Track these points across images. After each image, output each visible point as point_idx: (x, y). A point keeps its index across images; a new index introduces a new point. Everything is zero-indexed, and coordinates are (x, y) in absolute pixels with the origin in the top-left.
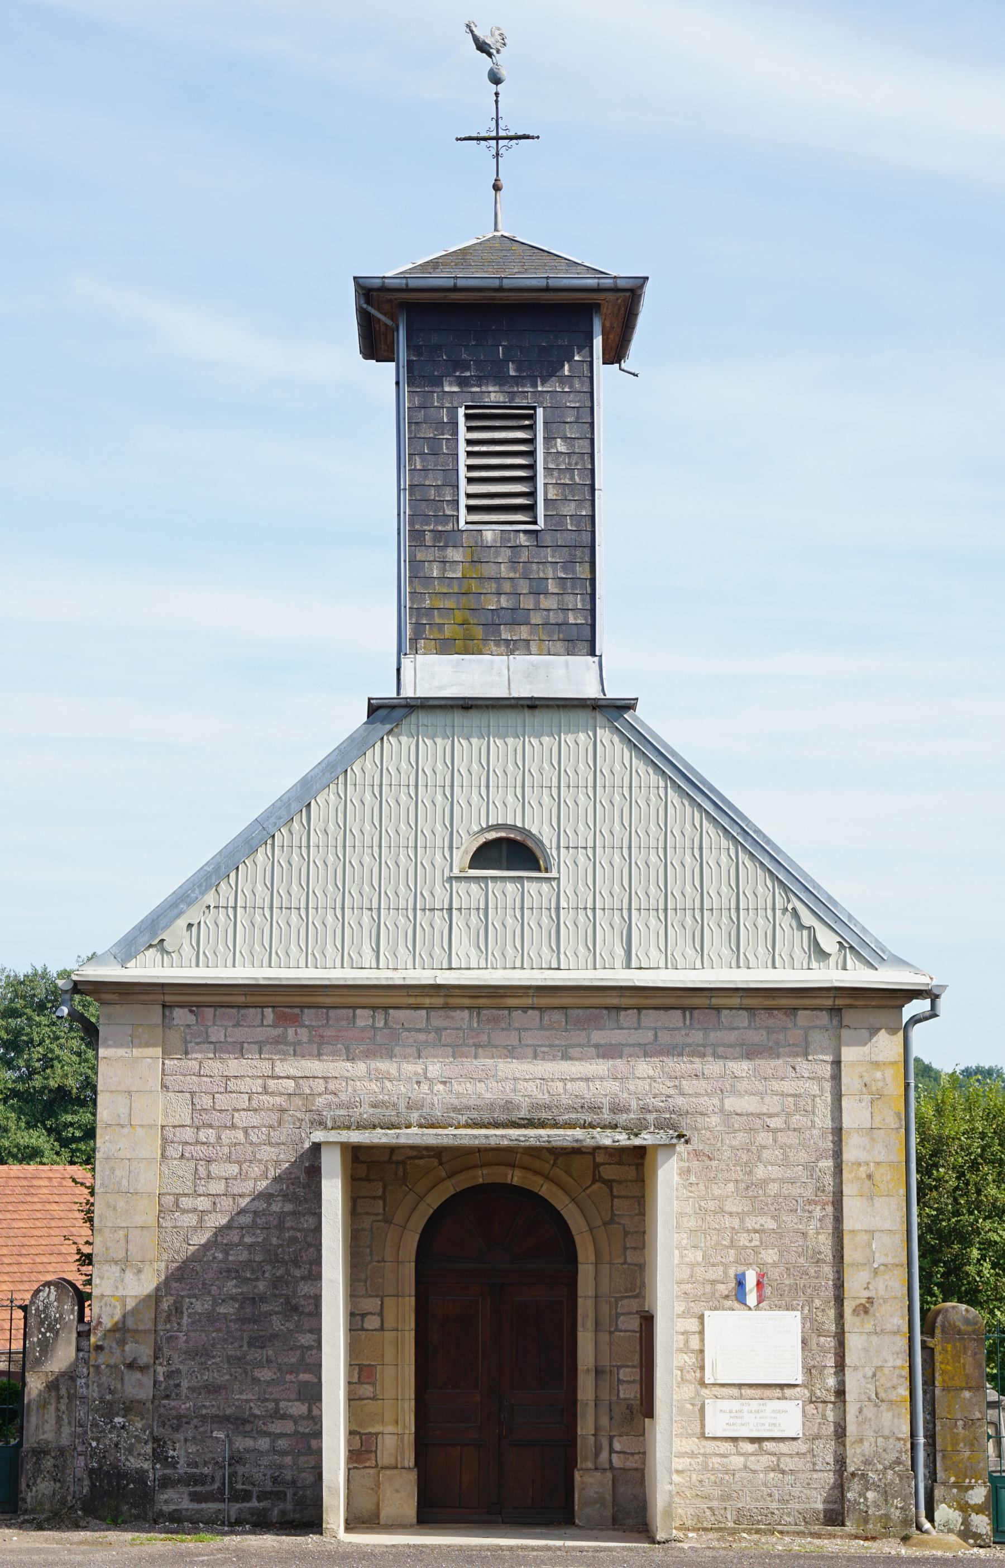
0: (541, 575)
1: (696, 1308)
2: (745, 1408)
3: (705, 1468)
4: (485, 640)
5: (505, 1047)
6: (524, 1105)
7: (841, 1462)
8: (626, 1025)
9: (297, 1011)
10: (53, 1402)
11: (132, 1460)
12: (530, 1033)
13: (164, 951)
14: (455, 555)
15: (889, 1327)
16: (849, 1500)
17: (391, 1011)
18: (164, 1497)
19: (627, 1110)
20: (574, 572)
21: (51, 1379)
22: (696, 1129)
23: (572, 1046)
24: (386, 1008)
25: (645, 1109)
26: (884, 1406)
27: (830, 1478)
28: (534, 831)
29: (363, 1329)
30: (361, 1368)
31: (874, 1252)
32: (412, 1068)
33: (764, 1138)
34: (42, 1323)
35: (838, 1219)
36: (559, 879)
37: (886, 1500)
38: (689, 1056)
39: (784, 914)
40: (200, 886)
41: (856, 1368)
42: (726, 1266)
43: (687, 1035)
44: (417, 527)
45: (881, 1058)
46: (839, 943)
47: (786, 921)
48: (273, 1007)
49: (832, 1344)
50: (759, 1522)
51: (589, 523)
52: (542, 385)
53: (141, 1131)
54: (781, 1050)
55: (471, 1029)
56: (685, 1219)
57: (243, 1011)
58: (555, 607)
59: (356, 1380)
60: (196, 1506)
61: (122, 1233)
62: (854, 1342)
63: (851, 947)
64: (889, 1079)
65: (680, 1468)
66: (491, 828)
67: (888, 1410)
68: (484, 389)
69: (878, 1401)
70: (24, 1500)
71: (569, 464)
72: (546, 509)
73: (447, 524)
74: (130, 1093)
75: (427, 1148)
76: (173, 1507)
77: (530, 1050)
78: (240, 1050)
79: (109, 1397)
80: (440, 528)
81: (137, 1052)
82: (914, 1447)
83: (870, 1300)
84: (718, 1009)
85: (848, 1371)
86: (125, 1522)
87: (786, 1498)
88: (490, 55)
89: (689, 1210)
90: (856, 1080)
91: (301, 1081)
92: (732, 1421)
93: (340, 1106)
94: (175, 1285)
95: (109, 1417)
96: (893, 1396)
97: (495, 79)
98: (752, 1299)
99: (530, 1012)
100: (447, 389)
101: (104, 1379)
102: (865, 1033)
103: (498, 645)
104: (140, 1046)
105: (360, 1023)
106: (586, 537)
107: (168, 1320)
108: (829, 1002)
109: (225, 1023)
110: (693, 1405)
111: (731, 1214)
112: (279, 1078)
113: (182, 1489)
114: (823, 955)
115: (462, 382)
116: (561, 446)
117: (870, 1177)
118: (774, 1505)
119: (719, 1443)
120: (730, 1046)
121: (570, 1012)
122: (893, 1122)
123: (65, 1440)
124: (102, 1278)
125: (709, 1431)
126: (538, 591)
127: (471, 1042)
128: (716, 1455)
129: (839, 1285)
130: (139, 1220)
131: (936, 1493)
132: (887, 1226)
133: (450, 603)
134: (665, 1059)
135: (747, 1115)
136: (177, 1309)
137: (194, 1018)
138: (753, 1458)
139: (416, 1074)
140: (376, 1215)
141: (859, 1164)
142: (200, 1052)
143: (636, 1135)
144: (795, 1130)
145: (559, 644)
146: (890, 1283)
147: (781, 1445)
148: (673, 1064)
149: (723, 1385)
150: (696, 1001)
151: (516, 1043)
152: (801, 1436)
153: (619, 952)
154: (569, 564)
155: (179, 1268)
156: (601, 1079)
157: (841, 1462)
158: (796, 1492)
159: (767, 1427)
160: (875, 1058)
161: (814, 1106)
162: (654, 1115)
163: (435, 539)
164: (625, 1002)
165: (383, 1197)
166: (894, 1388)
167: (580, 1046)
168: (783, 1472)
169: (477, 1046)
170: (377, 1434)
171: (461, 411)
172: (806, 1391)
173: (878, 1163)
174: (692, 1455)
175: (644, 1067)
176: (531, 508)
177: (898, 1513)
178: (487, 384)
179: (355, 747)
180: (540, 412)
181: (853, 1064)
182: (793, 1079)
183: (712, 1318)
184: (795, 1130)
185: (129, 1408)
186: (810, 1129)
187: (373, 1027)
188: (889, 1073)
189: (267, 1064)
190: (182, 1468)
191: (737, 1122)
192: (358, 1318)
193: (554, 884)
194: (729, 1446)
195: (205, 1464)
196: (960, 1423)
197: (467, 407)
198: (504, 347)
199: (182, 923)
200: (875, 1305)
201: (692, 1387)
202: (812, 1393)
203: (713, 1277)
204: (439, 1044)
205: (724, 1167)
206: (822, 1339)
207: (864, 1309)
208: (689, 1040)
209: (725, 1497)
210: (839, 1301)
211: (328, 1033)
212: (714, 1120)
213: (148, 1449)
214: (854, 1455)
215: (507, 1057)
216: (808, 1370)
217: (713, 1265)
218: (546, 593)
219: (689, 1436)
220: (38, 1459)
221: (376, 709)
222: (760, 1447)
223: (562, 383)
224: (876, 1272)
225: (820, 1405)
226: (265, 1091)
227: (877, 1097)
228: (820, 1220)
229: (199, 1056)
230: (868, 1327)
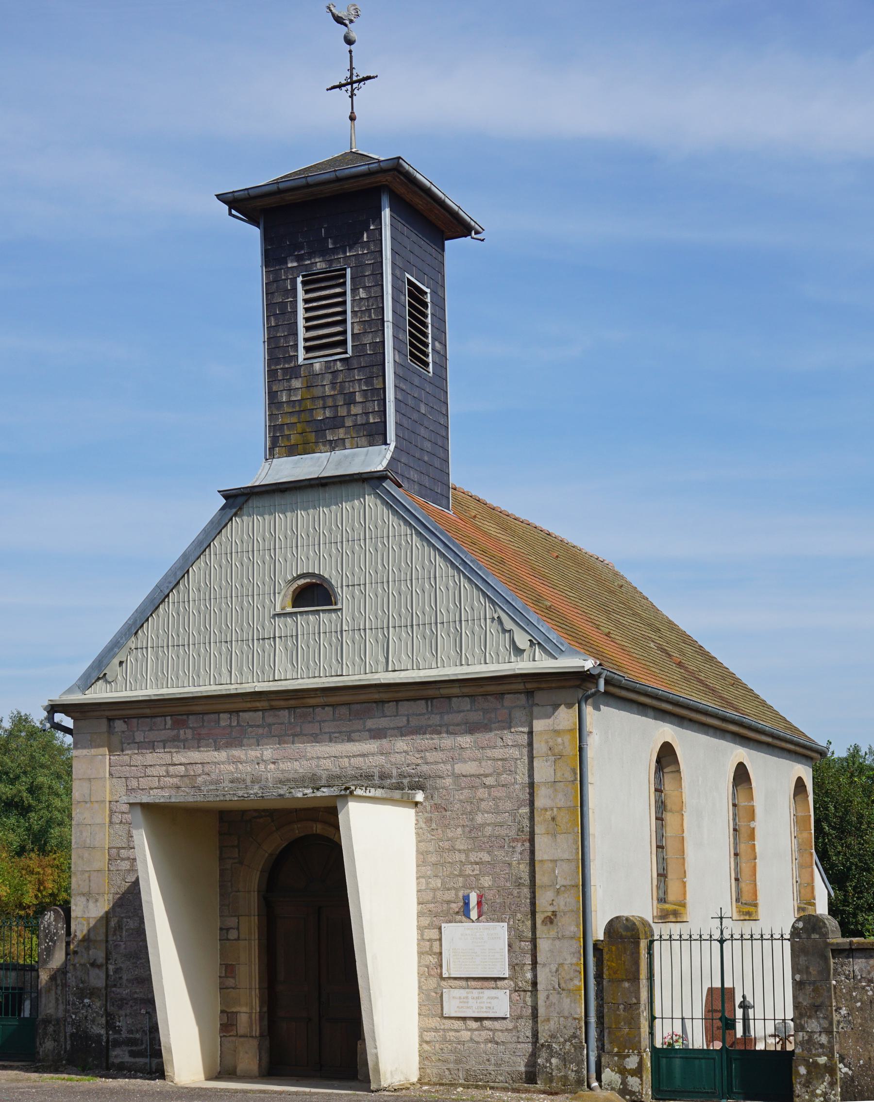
0: (351, 390)
1: (436, 921)
2: (470, 996)
3: (445, 1040)
4: (316, 443)
5: (312, 735)
6: (324, 776)
7: (535, 1035)
8: (388, 714)
9: (185, 717)
10: (54, 988)
11: (95, 1028)
12: (327, 723)
13: (107, 682)
14: (296, 383)
15: (567, 933)
16: (539, 1065)
17: (241, 714)
18: (114, 1053)
19: (390, 777)
20: (372, 384)
21: (52, 973)
22: (436, 789)
23: (354, 732)
24: (238, 712)
25: (401, 775)
26: (564, 994)
27: (529, 1047)
28: (326, 576)
29: (228, 940)
30: (227, 966)
31: (557, 877)
32: (253, 753)
33: (482, 793)
34: (46, 936)
35: (532, 852)
36: (341, 609)
37: (565, 1065)
38: (430, 734)
39: (492, 622)
40: (126, 634)
41: (544, 965)
42: (457, 890)
43: (429, 718)
44: (273, 367)
45: (561, 727)
46: (530, 640)
47: (493, 628)
48: (171, 715)
49: (530, 947)
50: (481, 1080)
51: (381, 347)
52: (350, 251)
53: (96, 805)
54: (493, 726)
55: (290, 723)
56: (429, 856)
57: (154, 720)
58: (360, 412)
59: (223, 975)
60: (133, 1060)
61: (87, 875)
62: (543, 945)
63: (539, 643)
64: (567, 744)
65: (428, 1039)
66: (300, 577)
67: (567, 997)
68: (313, 261)
69: (560, 989)
70: (38, 1052)
71: (368, 306)
72: (353, 341)
73: (291, 362)
74: (90, 779)
76: (119, 1060)
77: (327, 736)
78: (151, 746)
79: (81, 985)
80: (287, 366)
81: (94, 751)
82: (587, 1024)
83: (554, 913)
84: (449, 698)
85: (539, 968)
86: (90, 1069)
87: (500, 1062)
88: (346, 25)
89: (431, 849)
90: (543, 745)
91: (188, 767)
92: (462, 1005)
93: (211, 783)
94: (118, 910)
95: (81, 999)
96: (571, 986)
97: (349, 41)
98: (474, 914)
99: (327, 708)
100: (290, 265)
101: (78, 973)
102: (550, 709)
103: (324, 445)
104: (95, 747)
105: (223, 724)
106: (379, 357)
107: (115, 934)
108: (521, 687)
109: (144, 729)
110: (436, 993)
111: (459, 851)
112: (176, 765)
113: (125, 1048)
114: (519, 652)
115: (299, 259)
116: (362, 294)
117: (553, 819)
118: (491, 1068)
119: (453, 1021)
120: (458, 725)
121: (352, 706)
122: (569, 776)
123: (61, 1014)
124: (76, 905)
125: (446, 1013)
126: (350, 401)
127: (290, 732)
128: (451, 1030)
129: (533, 904)
130: (97, 865)
131: (603, 1060)
132: (566, 856)
133: (294, 419)
134: (414, 737)
135: (471, 776)
136: (119, 927)
137: (125, 726)
138: (476, 1033)
139: (257, 757)
140: (234, 859)
141: (546, 810)
142: (130, 749)
143: (318, 789)
144: (503, 786)
145: (363, 439)
146: (568, 900)
147: (496, 1023)
148: (424, 741)
149: (455, 979)
150: (430, 692)
151: (318, 732)
152: (508, 1016)
153: (382, 659)
154: (369, 380)
155: (120, 899)
156: (373, 754)
157: (535, 1035)
158: (506, 1057)
159: (484, 1010)
160: (557, 728)
161: (516, 767)
162: (408, 779)
163: (284, 374)
164: (384, 696)
166: (571, 980)
167: (359, 731)
168: (497, 1043)
169: (294, 735)
170: (236, 1013)
171: (300, 279)
172: (512, 983)
173: (559, 808)
174: (436, 1030)
175: (401, 744)
176: (344, 343)
177: (573, 1074)
178: (314, 257)
179: (217, 527)
180: (349, 271)
181: (541, 733)
182: (501, 747)
183: (448, 929)
184: (503, 786)
185: (93, 993)
186: (513, 784)
187: (230, 726)
188: (567, 738)
189: (168, 756)
190: (124, 1034)
191: (464, 782)
192: (225, 931)
193: (339, 613)
194: (458, 1024)
195: (137, 1031)
196: (621, 1007)
197: (303, 276)
198: (325, 228)
199: (116, 661)
200: (558, 917)
201: (435, 980)
202: (516, 984)
203: (449, 899)
204: (270, 735)
205: (455, 816)
206: (523, 943)
207: (550, 920)
208: (430, 722)
209: (458, 1061)
210: (533, 913)
211: (204, 731)
212: (448, 781)
213: (103, 1021)
214: (544, 1031)
215: (313, 742)
216: (513, 966)
217: (449, 890)
218: (355, 403)
219: (434, 1016)
220: (46, 1026)
221: (238, 500)
222: (482, 1025)
223: (363, 248)
224: (558, 892)
225: (522, 993)
226: (168, 775)
227: (558, 757)
228: (521, 854)
229: (129, 752)
230: (553, 934)
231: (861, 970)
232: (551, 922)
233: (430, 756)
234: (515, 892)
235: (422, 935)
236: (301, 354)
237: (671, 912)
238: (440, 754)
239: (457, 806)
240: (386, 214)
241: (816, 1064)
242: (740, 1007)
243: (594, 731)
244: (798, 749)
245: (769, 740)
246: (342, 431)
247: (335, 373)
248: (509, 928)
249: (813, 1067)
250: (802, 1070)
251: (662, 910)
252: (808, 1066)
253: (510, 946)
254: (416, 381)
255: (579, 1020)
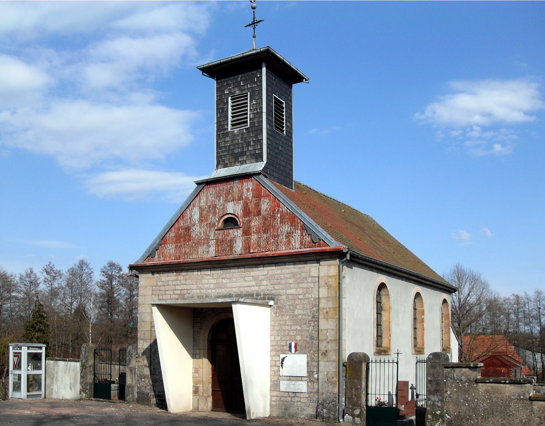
3: (280, 400)
14: (228, 139)
15: (332, 359)
25: (265, 295)
33: (297, 302)
42: (286, 341)
62: (321, 363)
69: (328, 381)
75: (210, 308)
83: (326, 351)
89: (277, 324)
95: (141, 379)
96: (333, 380)
111: (288, 325)
116: (254, 102)
117: (327, 312)
126: (248, 145)
132: (332, 328)
133: (226, 153)
160: (329, 275)
165: (200, 322)
171: (230, 98)
173: (329, 308)
176: (246, 122)
180: (249, 93)
188: (333, 279)
191: (290, 297)
216: (308, 372)
224: (328, 342)
227: (329, 287)
230: (326, 359)
231: (457, 376)
232: (325, 355)
233: (277, 287)
234: (310, 342)
235: (272, 359)
236: (230, 127)
237: (382, 350)
238: (281, 286)
239: (287, 307)
240: (264, 70)
241: (436, 414)
242: (411, 389)
243: (347, 276)
244: (444, 288)
245: (431, 284)
246: (245, 157)
247: (243, 134)
248: (307, 357)
249: (435, 416)
250: (430, 416)
251: (378, 350)
252: (432, 415)
253: (308, 363)
254: (278, 137)
255: (336, 394)
